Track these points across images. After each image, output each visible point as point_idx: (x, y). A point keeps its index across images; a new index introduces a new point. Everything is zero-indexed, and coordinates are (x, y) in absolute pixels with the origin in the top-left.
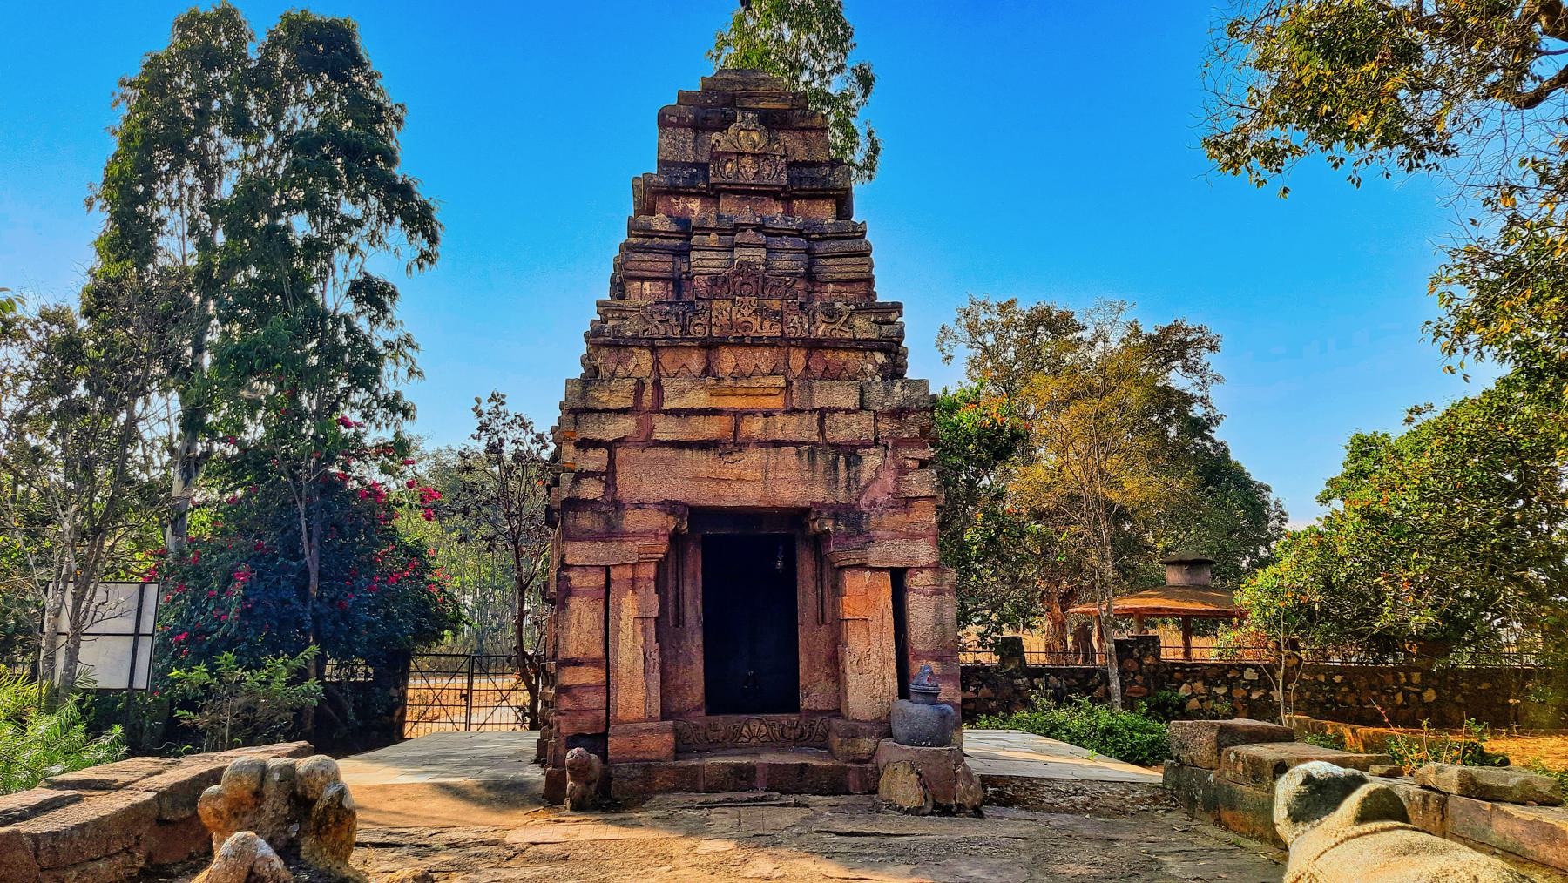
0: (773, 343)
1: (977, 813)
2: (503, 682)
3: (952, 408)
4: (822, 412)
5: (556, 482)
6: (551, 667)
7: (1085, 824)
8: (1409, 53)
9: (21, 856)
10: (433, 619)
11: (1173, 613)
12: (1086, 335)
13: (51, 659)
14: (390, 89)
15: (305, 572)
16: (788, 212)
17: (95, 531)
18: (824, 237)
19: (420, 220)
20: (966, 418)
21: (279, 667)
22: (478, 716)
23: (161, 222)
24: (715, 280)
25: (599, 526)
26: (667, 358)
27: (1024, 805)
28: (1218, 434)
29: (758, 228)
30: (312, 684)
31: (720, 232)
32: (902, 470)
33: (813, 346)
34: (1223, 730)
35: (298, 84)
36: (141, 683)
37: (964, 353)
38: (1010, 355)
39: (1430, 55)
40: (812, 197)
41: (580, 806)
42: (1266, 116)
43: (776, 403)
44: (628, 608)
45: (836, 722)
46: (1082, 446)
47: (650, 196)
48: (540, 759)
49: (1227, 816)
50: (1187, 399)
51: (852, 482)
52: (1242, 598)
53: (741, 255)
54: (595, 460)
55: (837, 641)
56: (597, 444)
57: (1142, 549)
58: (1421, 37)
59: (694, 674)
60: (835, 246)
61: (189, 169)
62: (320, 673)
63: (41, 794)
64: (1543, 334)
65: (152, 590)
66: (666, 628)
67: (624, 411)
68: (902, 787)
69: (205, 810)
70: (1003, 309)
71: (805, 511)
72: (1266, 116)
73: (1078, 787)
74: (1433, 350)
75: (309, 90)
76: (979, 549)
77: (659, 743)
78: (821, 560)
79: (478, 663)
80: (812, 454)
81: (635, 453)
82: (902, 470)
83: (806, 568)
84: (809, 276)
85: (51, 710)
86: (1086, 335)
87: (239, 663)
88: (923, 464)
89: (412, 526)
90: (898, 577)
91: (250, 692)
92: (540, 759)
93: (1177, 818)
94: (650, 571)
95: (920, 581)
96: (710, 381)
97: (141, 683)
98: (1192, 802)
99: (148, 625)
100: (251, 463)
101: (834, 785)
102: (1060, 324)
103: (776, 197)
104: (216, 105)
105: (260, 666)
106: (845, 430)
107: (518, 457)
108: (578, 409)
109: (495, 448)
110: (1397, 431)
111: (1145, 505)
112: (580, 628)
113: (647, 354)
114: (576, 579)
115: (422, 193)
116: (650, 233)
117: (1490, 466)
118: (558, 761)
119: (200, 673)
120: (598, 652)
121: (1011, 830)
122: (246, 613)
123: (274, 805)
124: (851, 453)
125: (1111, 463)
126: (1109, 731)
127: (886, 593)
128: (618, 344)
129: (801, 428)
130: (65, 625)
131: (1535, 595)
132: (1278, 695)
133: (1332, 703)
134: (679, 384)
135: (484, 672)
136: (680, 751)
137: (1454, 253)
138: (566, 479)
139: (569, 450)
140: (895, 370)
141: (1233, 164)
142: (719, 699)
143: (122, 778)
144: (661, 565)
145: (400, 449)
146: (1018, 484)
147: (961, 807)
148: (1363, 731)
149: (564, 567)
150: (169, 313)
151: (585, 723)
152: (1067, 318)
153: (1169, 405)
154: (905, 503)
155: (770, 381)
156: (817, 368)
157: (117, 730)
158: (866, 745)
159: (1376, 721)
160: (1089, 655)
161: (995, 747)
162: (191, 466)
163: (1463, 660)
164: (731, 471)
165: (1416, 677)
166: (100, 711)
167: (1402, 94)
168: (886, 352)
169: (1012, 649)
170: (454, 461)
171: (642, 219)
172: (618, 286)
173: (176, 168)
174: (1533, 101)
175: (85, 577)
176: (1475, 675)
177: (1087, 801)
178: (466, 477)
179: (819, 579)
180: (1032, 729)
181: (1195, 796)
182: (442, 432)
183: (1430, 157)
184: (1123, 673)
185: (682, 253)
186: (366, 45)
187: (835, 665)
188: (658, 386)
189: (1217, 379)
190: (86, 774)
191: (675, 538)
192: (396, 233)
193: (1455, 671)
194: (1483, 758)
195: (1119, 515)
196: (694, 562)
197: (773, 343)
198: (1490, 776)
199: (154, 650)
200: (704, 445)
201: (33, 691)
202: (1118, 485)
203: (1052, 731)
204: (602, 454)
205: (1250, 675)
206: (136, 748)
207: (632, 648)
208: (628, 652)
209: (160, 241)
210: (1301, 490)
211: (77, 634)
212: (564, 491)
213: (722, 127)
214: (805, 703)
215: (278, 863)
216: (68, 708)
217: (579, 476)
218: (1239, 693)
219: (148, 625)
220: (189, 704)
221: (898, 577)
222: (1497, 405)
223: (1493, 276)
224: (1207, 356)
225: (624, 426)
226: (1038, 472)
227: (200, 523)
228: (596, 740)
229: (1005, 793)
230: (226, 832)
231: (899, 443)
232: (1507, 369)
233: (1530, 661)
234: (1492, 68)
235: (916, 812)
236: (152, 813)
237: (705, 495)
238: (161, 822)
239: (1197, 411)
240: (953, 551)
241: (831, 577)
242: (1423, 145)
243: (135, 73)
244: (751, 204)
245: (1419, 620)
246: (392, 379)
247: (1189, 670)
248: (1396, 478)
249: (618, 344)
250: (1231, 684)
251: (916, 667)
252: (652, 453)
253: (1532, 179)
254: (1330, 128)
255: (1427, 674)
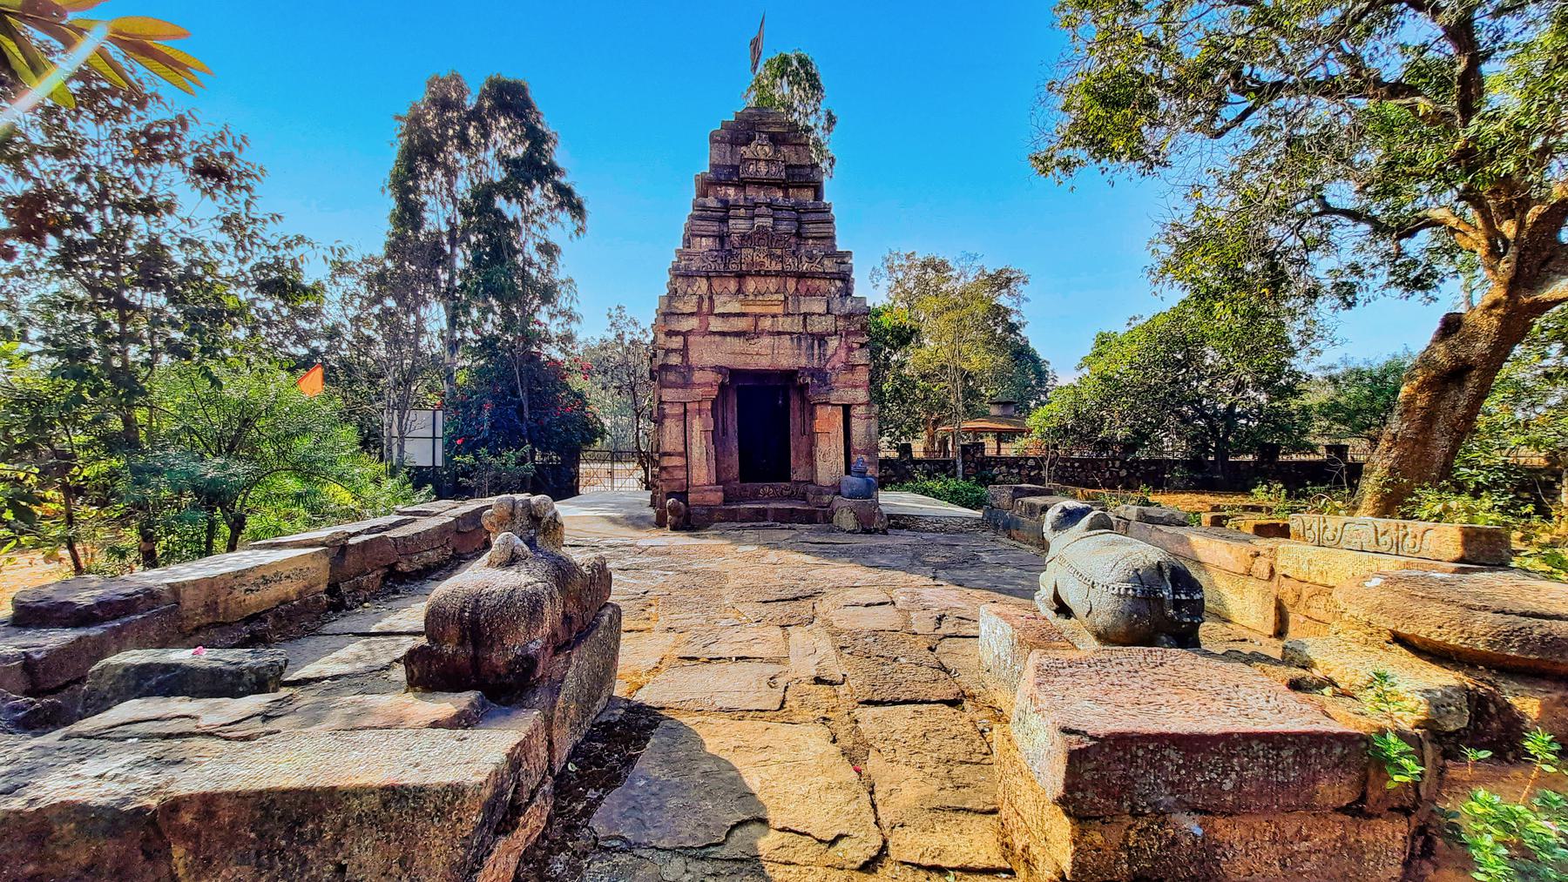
0: (777, 274)
1: (885, 532)
2: (630, 466)
3: (878, 314)
4: (805, 315)
5: (655, 355)
6: (656, 457)
7: (942, 538)
8: (1150, 104)
9: (390, 548)
10: (591, 432)
11: (993, 430)
12: (954, 274)
13: (390, 450)
14: (547, 125)
15: (521, 405)
16: (786, 196)
17: (406, 380)
18: (807, 212)
19: (577, 209)
20: (886, 321)
21: (510, 456)
22: (617, 484)
23: (425, 204)
24: (743, 237)
25: (680, 381)
26: (716, 283)
27: (909, 529)
28: (1023, 332)
29: (769, 205)
30: (529, 464)
31: (746, 207)
32: (850, 349)
33: (800, 276)
34: (1016, 489)
35: (496, 120)
36: (439, 463)
37: (885, 283)
38: (911, 284)
39: (1163, 106)
40: (800, 187)
41: (674, 528)
42: (1067, 142)
43: (779, 310)
44: (697, 425)
45: (811, 487)
46: (950, 338)
47: (706, 185)
48: (653, 505)
49: (1014, 533)
50: (1008, 312)
51: (822, 356)
52: (1031, 422)
53: (759, 222)
54: (677, 342)
55: (812, 444)
56: (677, 333)
57: (979, 396)
58: (1159, 93)
59: (734, 460)
60: (814, 217)
61: (438, 174)
62: (533, 459)
63: (395, 518)
64: (1208, 274)
65: (440, 414)
66: (718, 437)
67: (692, 314)
68: (846, 520)
69: (485, 522)
70: (908, 257)
71: (794, 373)
72: (1067, 142)
73: (938, 520)
74: (1146, 282)
75: (503, 124)
76: (893, 398)
77: (716, 497)
78: (804, 400)
79: (616, 456)
80: (799, 339)
81: (699, 339)
82: (850, 349)
83: (795, 404)
84: (798, 235)
85: (393, 477)
86: (954, 274)
87: (490, 453)
88: (862, 346)
89: (577, 382)
90: (847, 409)
91: (497, 469)
92: (653, 505)
93: (989, 534)
94: (709, 405)
95: (859, 411)
96: (741, 297)
97: (439, 463)
98: (997, 526)
99: (439, 433)
100: (488, 345)
101: (809, 518)
102: (939, 267)
103: (779, 186)
104: (451, 132)
105: (500, 455)
106: (818, 325)
107: (633, 342)
108: (667, 314)
109: (620, 337)
110: (1122, 330)
111: (982, 371)
112: (671, 437)
113: (704, 281)
114: (668, 409)
115: (579, 192)
116: (704, 208)
117: (1169, 350)
118: (662, 505)
119: (469, 459)
120: (681, 449)
121: (903, 541)
122: (492, 426)
123: (521, 520)
124: (821, 339)
125: (964, 348)
126: (955, 492)
127: (840, 417)
128: (688, 276)
129: (794, 325)
130: (395, 432)
131: (1185, 420)
132: (1044, 473)
133: (1074, 475)
134: (723, 298)
135: (619, 460)
136: (726, 501)
137: (1164, 226)
138: (660, 353)
139: (662, 336)
140: (846, 292)
141: (1045, 170)
142: (745, 475)
143: (436, 510)
144: (714, 402)
145: (568, 338)
146: (913, 360)
147: (876, 530)
148: (1086, 491)
149: (661, 402)
150: (435, 255)
151: (675, 486)
152: (943, 263)
153: (999, 314)
154: (851, 368)
155: (775, 297)
156: (803, 290)
157: (430, 487)
158: (827, 499)
159: (1095, 486)
160: (946, 452)
161: (894, 500)
162: (453, 346)
163: (1142, 455)
164: (753, 349)
165: (1117, 463)
166: (419, 478)
167: (1144, 129)
168: (843, 280)
169: (906, 450)
170: (596, 344)
171: (701, 200)
172: (687, 242)
173: (431, 171)
174: (1219, 135)
175: (402, 407)
176: (1150, 462)
177: (942, 527)
178: (603, 353)
179: (802, 410)
180: (914, 491)
181: (1000, 524)
182: (591, 332)
183: (1156, 168)
184: (964, 462)
185: (724, 220)
186: (534, 95)
187: (811, 456)
188: (711, 298)
189: (1027, 300)
190: (416, 508)
191: (722, 387)
192: (564, 216)
193: (1137, 460)
194: (1148, 504)
195: (967, 377)
196: (734, 401)
197: (777, 274)
198: (1152, 511)
199: (445, 446)
200: (738, 334)
201: (382, 466)
202: (968, 360)
203: (925, 492)
204: (680, 339)
205: (1031, 463)
206: (440, 495)
207: (699, 447)
208: (699, 457)
209: (425, 215)
210: (1067, 365)
211: (402, 437)
212: (658, 361)
213: (747, 144)
214: (794, 477)
215: (526, 548)
216: (402, 475)
217: (668, 352)
218: (1024, 472)
219: (439, 433)
220: (466, 474)
221: (847, 409)
222: (1178, 317)
223: (1185, 240)
224: (1021, 287)
225: (693, 323)
226: (924, 352)
227: (461, 378)
228: (682, 495)
229: (900, 523)
230: (498, 532)
231: (848, 333)
232: (1186, 295)
233: (1178, 456)
234: (1198, 112)
235: (852, 532)
236: (454, 527)
237: (739, 363)
238: (459, 532)
239: (1013, 319)
240: (877, 396)
241: (809, 410)
242: (1151, 161)
243: (405, 112)
244: (765, 195)
245: (1120, 434)
246: (563, 302)
247: (999, 460)
248: (1118, 356)
249: (688, 276)
250: (1021, 467)
251: (854, 458)
252: (708, 338)
253: (1213, 181)
254: (1101, 149)
255: (1123, 462)
